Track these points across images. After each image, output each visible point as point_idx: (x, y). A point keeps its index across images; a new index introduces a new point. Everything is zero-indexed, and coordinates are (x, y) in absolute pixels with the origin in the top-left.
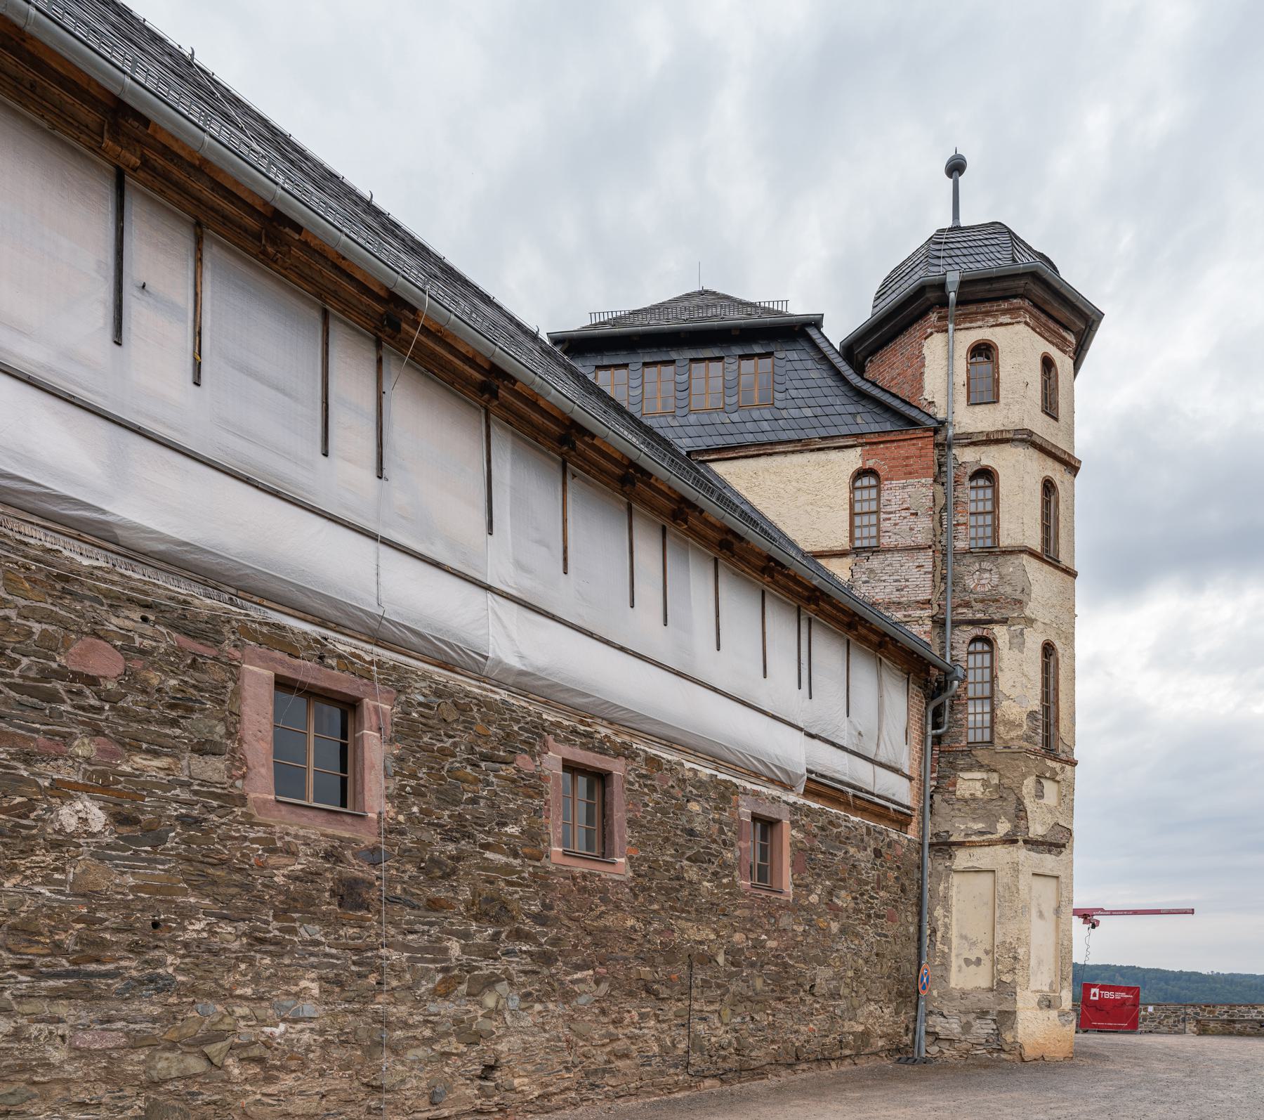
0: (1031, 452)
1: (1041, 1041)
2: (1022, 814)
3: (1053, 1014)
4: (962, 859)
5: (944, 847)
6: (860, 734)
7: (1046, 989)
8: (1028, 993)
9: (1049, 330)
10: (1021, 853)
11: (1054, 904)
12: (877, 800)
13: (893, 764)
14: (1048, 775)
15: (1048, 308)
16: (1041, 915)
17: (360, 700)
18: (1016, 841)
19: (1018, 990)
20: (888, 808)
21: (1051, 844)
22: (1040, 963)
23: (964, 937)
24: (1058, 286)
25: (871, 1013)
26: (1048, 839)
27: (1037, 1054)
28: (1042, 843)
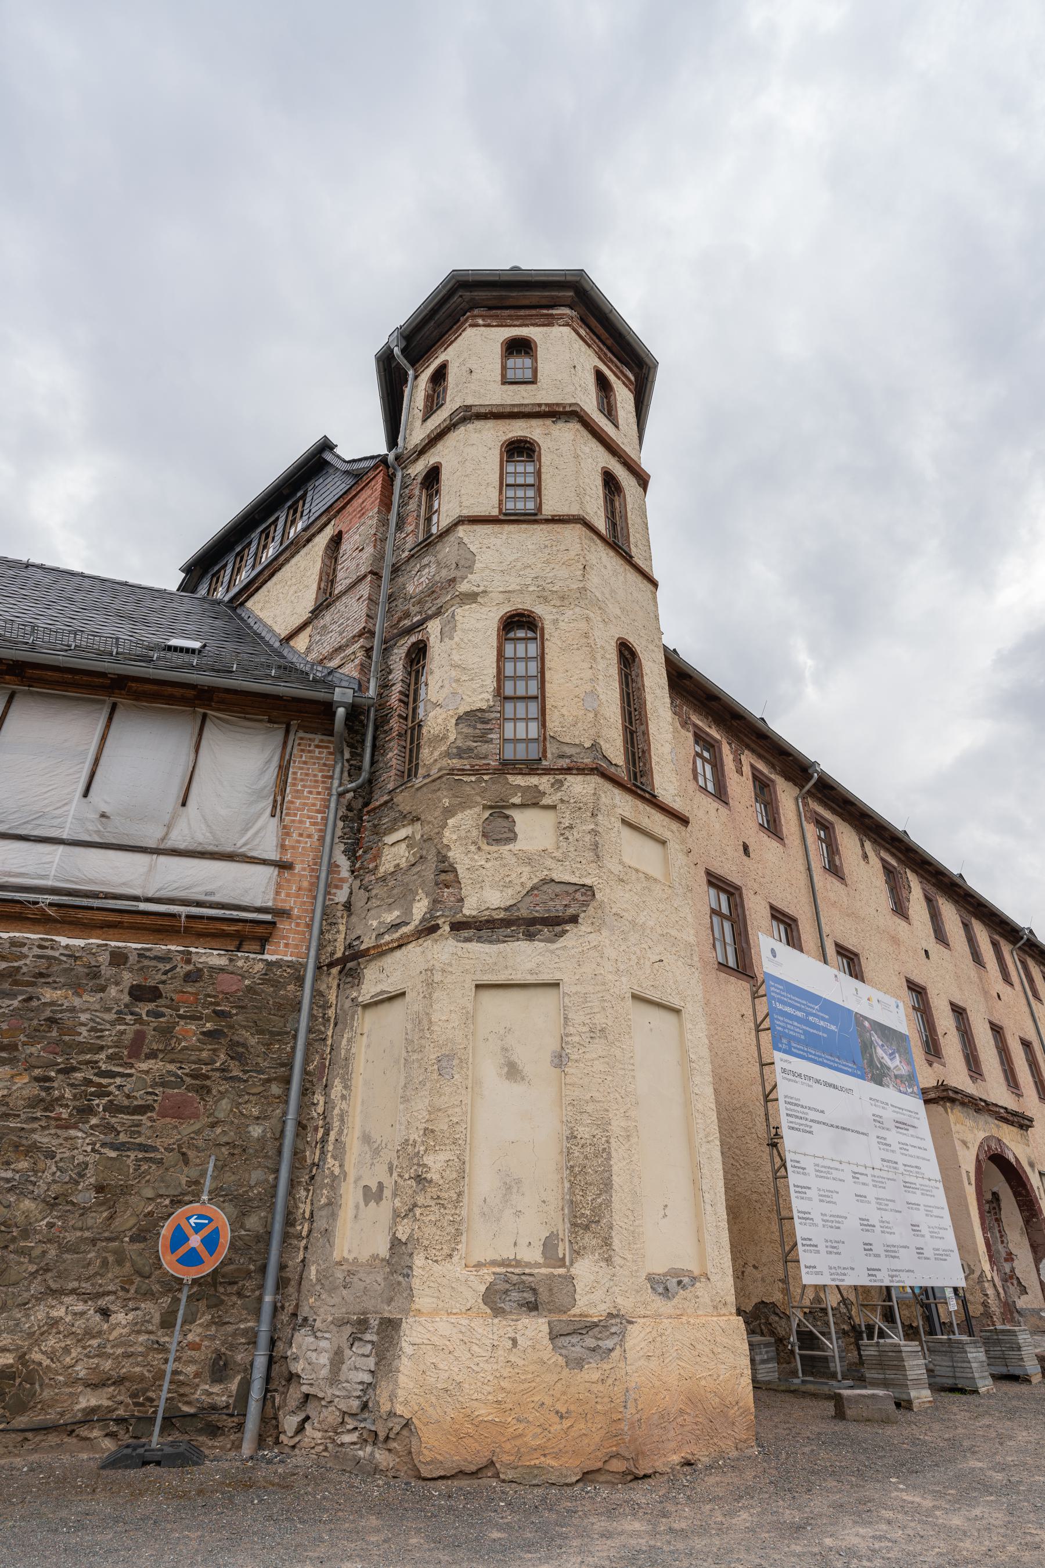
0: (479, 424)
1: (483, 1411)
2: (449, 877)
3: (534, 1329)
4: (374, 980)
5: (350, 964)
6: (103, 815)
7: (534, 1255)
8: (455, 1269)
9: (518, 318)
10: (444, 949)
11: (554, 1045)
12: (143, 906)
13: (211, 848)
14: (517, 800)
15: (511, 302)
16: (513, 1071)
17: (451, 930)
18: (435, 928)
19: (419, 1261)
20: (173, 916)
21: (533, 922)
22: (510, 1186)
23: (366, 1139)
24: (563, 279)
25: (54, 1323)
26: (524, 913)
27: (470, 1455)
28: (506, 923)
